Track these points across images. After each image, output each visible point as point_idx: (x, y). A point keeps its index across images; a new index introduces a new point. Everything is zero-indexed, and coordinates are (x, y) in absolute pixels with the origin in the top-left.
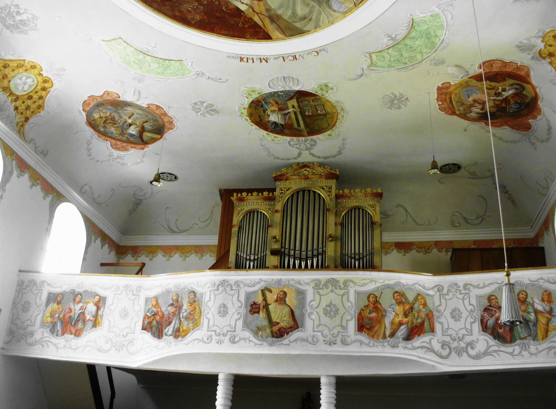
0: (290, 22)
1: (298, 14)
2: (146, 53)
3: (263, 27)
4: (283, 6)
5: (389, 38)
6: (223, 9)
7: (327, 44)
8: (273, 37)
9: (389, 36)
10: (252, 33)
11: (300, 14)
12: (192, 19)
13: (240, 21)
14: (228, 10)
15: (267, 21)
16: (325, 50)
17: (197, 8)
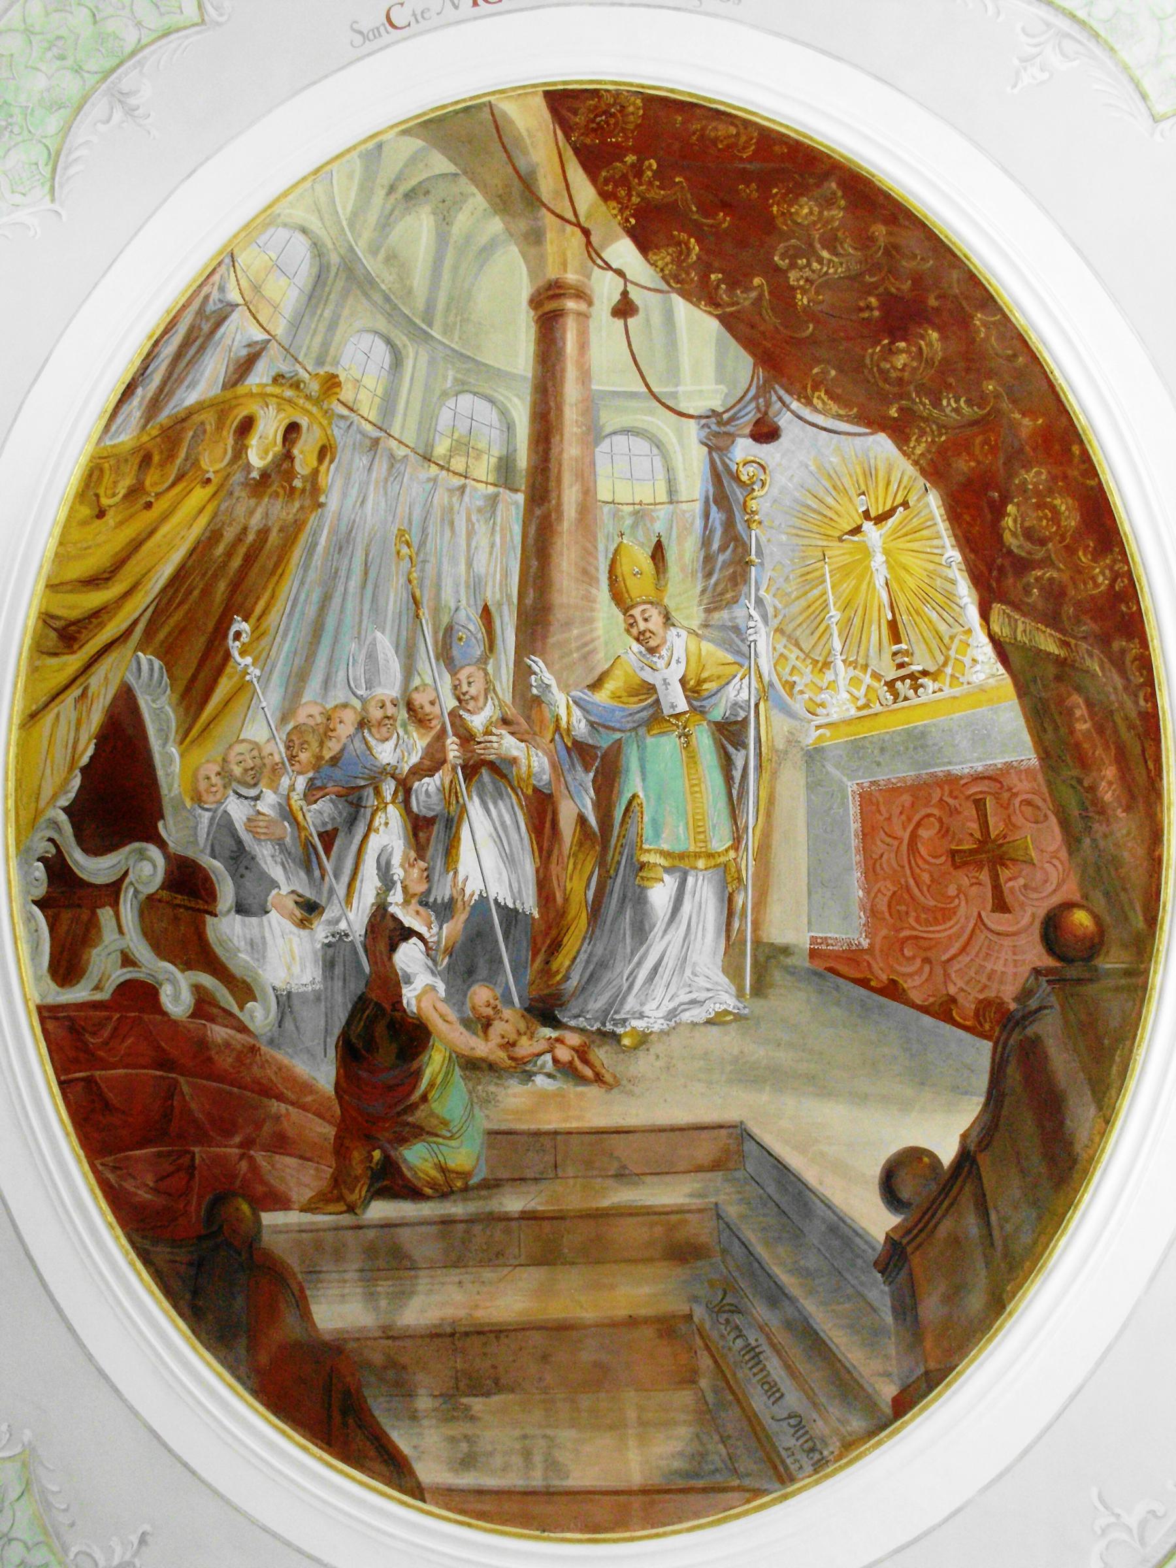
0: (464, 180)
1: (432, 217)
2: (1074, 30)
3: (569, 154)
4: (480, 253)
5: (133, 101)
6: (697, 248)
7: (351, 63)
8: (540, 103)
9: (130, 111)
10: (616, 124)
11: (423, 216)
12: (830, 202)
13: (650, 183)
14: (679, 243)
15: (547, 186)
16: (361, 33)
17: (793, 256)
